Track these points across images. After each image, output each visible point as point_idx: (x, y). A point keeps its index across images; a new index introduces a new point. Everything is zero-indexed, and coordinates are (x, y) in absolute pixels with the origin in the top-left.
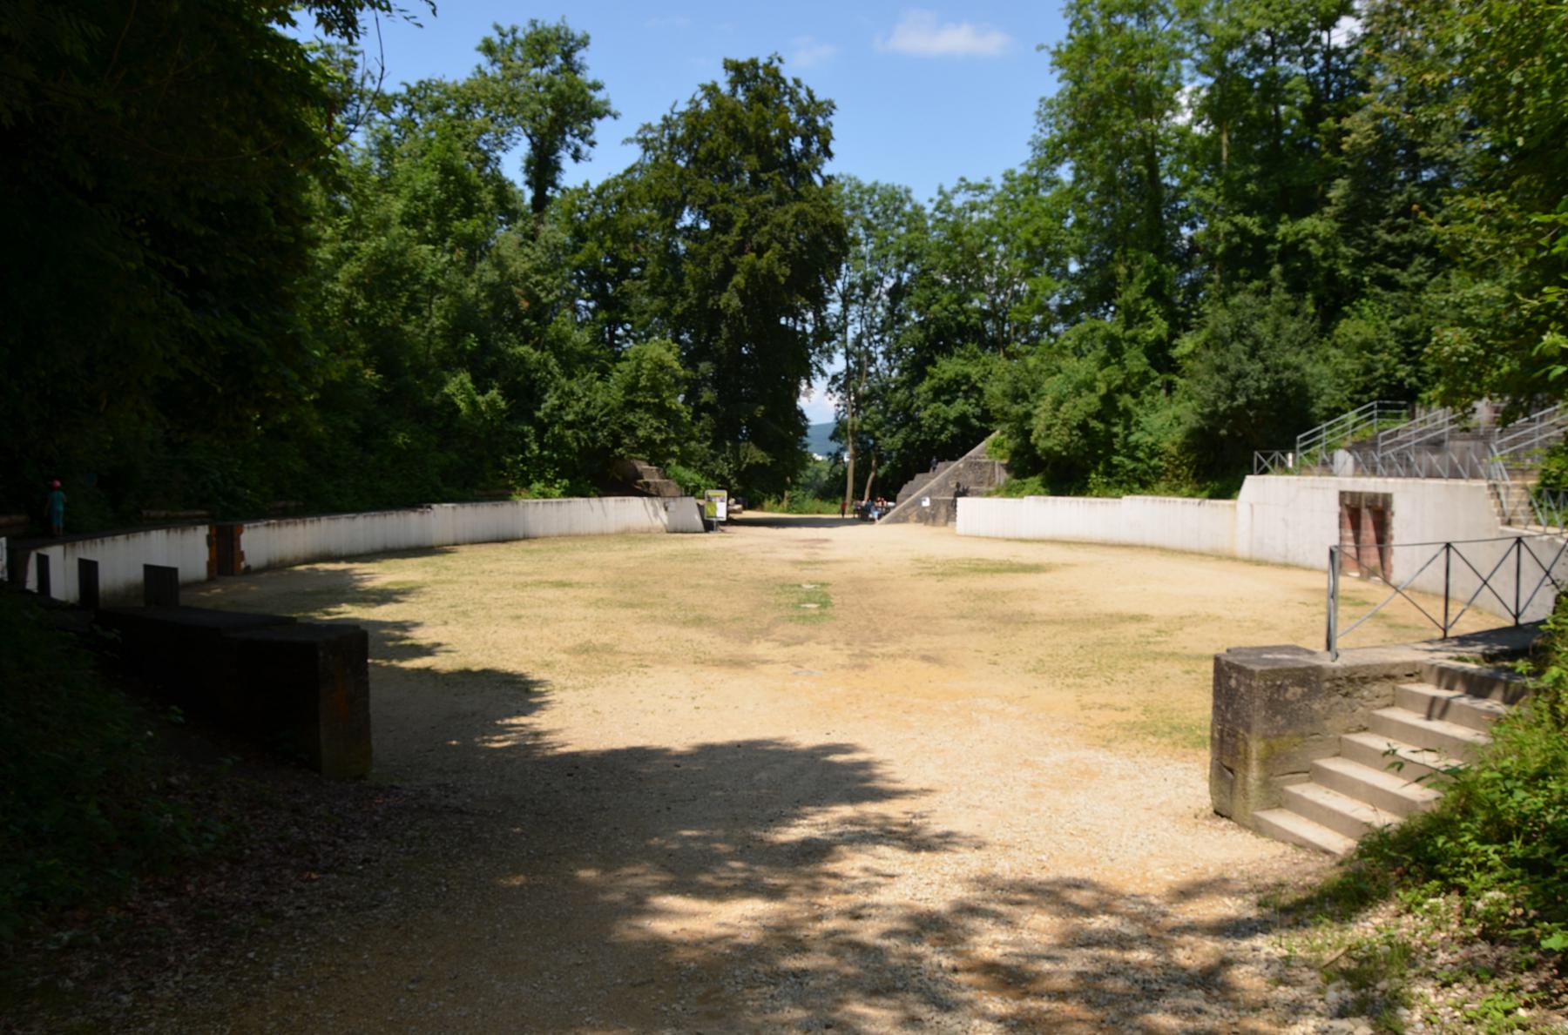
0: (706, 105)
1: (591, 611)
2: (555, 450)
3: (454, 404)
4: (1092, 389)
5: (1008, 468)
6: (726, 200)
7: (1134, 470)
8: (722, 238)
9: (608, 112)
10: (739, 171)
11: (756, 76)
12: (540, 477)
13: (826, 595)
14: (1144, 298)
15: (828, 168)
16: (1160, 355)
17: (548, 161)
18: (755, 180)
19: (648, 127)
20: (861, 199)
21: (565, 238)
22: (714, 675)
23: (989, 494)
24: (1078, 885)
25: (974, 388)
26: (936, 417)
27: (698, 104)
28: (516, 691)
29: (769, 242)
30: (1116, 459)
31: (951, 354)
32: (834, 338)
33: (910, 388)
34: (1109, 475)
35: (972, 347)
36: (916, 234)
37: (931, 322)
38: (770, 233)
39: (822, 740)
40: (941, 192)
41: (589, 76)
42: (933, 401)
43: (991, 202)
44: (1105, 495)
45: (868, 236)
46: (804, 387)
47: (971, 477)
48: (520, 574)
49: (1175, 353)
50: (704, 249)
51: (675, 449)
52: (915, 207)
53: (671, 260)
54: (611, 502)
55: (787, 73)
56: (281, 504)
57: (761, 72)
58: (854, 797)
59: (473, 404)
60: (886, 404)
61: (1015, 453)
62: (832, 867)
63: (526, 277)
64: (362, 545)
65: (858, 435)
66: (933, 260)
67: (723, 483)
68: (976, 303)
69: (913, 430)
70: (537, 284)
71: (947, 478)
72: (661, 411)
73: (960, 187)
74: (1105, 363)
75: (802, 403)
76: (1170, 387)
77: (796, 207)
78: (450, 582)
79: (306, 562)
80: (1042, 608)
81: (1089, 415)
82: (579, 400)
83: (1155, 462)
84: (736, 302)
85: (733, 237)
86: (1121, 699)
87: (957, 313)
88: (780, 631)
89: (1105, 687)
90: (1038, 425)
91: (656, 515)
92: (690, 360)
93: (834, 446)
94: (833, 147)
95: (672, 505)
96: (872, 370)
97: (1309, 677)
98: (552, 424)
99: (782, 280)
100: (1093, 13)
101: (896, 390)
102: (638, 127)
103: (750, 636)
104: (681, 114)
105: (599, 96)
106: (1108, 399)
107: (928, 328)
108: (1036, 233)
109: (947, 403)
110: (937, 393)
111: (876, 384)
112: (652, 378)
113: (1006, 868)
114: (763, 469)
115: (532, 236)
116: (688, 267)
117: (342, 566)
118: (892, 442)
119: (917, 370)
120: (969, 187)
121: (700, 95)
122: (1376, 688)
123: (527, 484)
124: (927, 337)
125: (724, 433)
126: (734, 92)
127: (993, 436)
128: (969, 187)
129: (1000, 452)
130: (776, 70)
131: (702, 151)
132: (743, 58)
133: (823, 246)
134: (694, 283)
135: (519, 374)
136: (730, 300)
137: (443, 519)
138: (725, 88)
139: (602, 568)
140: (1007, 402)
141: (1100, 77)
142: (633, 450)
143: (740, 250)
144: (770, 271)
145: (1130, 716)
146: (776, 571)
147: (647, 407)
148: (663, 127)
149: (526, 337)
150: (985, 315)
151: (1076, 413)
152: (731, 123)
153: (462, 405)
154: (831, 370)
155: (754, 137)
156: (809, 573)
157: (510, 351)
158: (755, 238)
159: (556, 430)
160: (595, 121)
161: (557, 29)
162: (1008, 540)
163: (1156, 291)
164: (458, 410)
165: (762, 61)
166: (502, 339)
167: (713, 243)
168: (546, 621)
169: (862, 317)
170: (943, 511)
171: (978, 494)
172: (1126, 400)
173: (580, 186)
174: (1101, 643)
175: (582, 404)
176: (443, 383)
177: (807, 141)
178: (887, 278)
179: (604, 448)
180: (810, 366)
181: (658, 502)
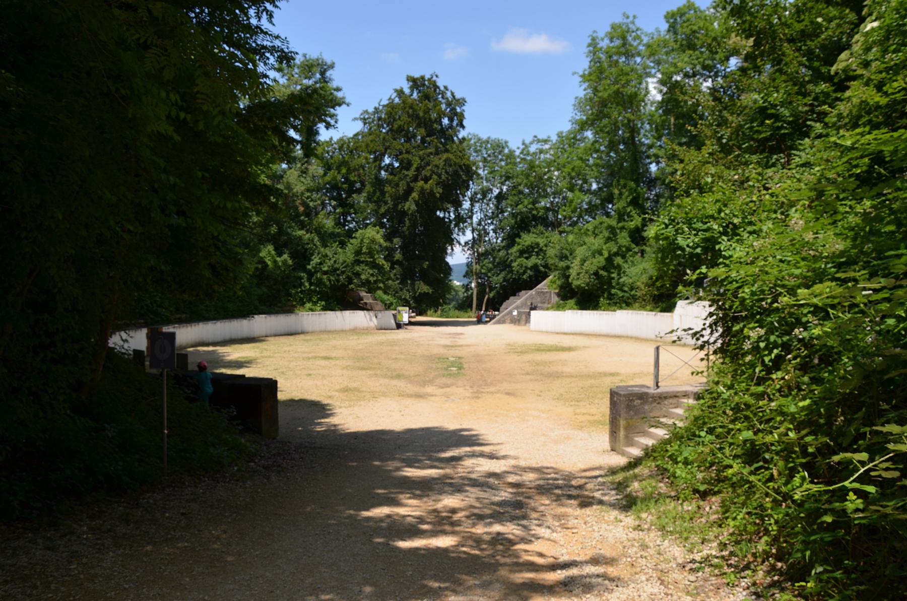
0: (397, 100)
1: (345, 372)
2: (317, 286)
3: (265, 262)
4: (601, 254)
5: (558, 295)
6: (408, 152)
7: (623, 297)
8: (406, 173)
9: (344, 103)
10: (414, 136)
11: (424, 85)
12: (310, 300)
13: (461, 363)
14: (628, 206)
15: (462, 134)
16: (637, 237)
17: (312, 129)
18: (423, 141)
19: (366, 112)
20: (481, 146)
21: (321, 171)
22: (409, 401)
23: (548, 309)
24: (548, 468)
25: (541, 250)
26: (521, 266)
27: (393, 100)
28: (319, 409)
29: (431, 175)
30: (613, 291)
31: (529, 231)
32: (466, 222)
33: (507, 250)
34: (610, 299)
35: (541, 228)
36: (510, 166)
37: (518, 214)
38: (431, 170)
39: (458, 427)
40: (523, 144)
41: (334, 84)
42: (519, 257)
43: (550, 148)
44: (608, 310)
45: (485, 166)
46: (449, 251)
47: (539, 299)
48: (304, 352)
49: (645, 234)
50: (396, 178)
51: (381, 285)
52: (510, 151)
53: (379, 183)
54: (347, 314)
55: (441, 83)
56: (178, 316)
57: (426, 83)
58: (470, 445)
59: (275, 262)
60: (494, 258)
61: (561, 287)
62: (463, 463)
63: (302, 194)
64: (219, 337)
65: (479, 275)
66: (520, 181)
67: (406, 303)
68: (543, 203)
69: (509, 273)
70: (308, 198)
71: (526, 299)
72: (374, 265)
73: (534, 141)
74: (608, 239)
75: (449, 259)
76: (643, 252)
77: (445, 156)
78: (270, 357)
79: (192, 346)
80: (567, 370)
81: (599, 268)
82: (330, 259)
83: (633, 292)
84: (413, 207)
85: (411, 173)
86: (594, 411)
87: (532, 209)
88: (438, 381)
89: (588, 406)
90: (573, 272)
91: (371, 320)
92: (388, 237)
93: (466, 281)
94: (465, 123)
95: (380, 315)
96: (487, 239)
97: (643, 397)
98: (316, 272)
99: (438, 195)
100: (601, 55)
101: (499, 250)
102: (361, 112)
103: (424, 384)
104: (384, 106)
105: (339, 95)
106: (609, 260)
107: (516, 218)
108: (573, 169)
109: (527, 258)
110: (522, 253)
111: (488, 247)
112: (369, 248)
113: (523, 463)
114: (424, 288)
115: (304, 172)
116: (388, 188)
117: (211, 348)
118: (497, 280)
119: (511, 240)
120: (539, 141)
121: (395, 94)
122: (671, 401)
123: (303, 304)
124: (516, 222)
125: (407, 276)
126: (412, 92)
127: (551, 277)
128: (539, 141)
129: (555, 286)
130: (435, 82)
131: (396, 126)
132: (417, 75)
133: (459, 176)
134: (391, 197)
135: (299, 245)
136: (410, 206)
137: (260, 323)
138: (407, 91)
139: (345, 349)
140: (557, 260)
141: (605, 89)
142: (359, 286)
143: (415, 179)
144: (432, 191)
145: (595, 418)
146: (435, 351)
147: (367, 263)
148: (374, 113)
149: (302, 226)
150: (547, 209)
151: (592, 266)
152: (411, 111)
153: (269, 263)
154: (463, 239)
155: (423, 117)
156: (452, 352)
157: (294, 233)
158: (424, 173)
159: (319, 275)
160: (337, 107)
161: (318, 60)
162: (557, 333)
163: (636, 202)
164: (267, 265)
165: (427, 76)
166: (290, 227)
167: (401, 175)
168: (324, 377)
169: (481, 210)
170: (524, 317)
171: (542, 309)
172: (618, 260)
173: (328, 139)
174: (592, 386)
175: (332, 262)
176: (260, 251)
177: (451, 120)
178: (495, 189)
179: (343, 285)
180: (453, 240)
181: (372, 313)
